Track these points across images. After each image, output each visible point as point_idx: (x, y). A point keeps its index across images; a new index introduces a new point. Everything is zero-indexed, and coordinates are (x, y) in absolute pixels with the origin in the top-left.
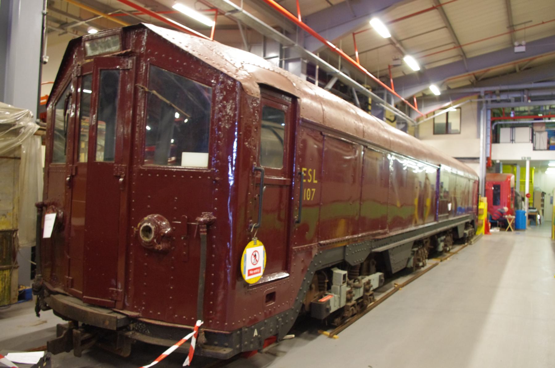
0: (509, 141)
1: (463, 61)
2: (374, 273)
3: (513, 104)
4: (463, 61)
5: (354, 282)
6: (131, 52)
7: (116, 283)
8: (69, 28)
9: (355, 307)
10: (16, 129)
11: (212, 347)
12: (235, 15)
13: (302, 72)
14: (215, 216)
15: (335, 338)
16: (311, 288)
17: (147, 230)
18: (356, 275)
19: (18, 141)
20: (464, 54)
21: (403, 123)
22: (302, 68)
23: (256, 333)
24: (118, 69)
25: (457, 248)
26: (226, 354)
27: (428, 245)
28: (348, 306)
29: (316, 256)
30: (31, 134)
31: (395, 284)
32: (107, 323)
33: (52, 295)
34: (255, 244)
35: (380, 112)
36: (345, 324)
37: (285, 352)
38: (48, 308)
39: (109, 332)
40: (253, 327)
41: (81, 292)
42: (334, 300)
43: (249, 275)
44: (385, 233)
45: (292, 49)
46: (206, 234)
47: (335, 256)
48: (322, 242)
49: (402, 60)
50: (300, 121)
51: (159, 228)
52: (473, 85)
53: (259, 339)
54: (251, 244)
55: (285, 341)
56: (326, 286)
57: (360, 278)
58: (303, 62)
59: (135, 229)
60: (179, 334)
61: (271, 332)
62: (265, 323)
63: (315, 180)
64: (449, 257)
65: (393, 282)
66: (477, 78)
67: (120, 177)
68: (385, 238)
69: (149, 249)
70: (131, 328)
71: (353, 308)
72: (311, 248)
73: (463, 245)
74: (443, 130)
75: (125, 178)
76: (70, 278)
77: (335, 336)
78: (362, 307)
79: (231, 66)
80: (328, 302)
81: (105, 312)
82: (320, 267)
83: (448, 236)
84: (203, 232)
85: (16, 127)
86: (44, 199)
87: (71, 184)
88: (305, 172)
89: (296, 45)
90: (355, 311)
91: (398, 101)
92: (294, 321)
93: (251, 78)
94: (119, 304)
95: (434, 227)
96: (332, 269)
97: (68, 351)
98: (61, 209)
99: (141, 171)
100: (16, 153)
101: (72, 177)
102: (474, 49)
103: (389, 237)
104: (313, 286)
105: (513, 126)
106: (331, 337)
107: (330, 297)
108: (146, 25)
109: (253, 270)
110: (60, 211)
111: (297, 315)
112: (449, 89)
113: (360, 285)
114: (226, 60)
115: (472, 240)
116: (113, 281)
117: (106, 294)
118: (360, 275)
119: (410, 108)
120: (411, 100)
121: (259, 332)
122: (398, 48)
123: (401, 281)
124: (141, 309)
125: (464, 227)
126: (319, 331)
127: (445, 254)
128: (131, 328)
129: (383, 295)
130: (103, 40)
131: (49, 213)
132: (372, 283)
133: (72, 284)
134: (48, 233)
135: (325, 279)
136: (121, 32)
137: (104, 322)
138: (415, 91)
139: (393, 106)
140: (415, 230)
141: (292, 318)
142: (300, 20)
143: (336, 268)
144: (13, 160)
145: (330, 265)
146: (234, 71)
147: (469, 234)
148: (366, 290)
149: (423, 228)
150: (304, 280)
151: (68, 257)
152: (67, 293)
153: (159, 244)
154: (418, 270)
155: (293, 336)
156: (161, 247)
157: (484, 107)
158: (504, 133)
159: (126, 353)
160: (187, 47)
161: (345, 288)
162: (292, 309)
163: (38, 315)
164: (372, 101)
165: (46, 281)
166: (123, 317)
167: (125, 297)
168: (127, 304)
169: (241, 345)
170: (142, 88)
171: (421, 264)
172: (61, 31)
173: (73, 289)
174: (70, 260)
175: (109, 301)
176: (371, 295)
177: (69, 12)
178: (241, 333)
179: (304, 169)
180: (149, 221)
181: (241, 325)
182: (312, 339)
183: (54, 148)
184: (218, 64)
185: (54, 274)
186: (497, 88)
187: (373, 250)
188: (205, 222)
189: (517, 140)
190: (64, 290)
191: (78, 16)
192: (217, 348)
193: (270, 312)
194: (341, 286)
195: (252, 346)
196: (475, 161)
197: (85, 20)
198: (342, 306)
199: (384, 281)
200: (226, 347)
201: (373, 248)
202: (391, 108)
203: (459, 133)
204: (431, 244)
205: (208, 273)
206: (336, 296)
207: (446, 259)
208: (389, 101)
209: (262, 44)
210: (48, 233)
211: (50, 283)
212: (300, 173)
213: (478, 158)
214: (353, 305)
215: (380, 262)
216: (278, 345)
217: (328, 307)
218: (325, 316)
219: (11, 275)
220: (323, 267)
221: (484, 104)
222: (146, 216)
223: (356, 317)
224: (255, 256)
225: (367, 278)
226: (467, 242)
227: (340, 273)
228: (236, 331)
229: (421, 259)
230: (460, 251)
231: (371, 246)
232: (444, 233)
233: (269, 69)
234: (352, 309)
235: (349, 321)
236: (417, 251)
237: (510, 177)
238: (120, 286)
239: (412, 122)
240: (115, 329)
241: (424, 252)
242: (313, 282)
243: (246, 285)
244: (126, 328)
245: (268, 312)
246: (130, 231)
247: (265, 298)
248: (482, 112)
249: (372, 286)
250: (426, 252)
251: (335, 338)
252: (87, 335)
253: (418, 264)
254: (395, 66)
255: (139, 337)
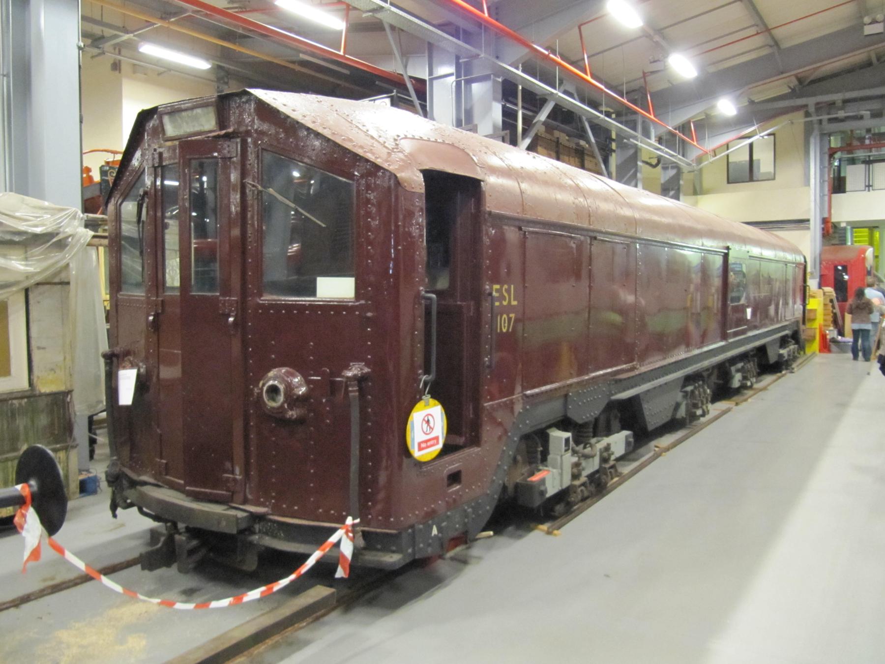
0: (862, 187)
1: (775, 56)
2: (618, 432)
3: (869, 122)
4: (775, 56)
5: (585, 448)
6: (233, 132)
7: (233, 467)
8: (107, 46)
9: (586, 487)
10: (60, 240)
11: (374, 553)
12: (379, 15)
13: (495, 99)
14: (369, 367)
15: (555, 535)
16: (515, 460)
17: (274, 390)
18: (588, 437)
19: (65, 258)
20: (776, 43)
21: (673, 168)
22: (494, 91)
23: (435, 531)
24: (216, 157)
25: (768, 379)
26: (395, 562)
27: (714, 379)
28: (575, 486)
29: (520, 413)
30: (82, 245)
31: (657, 447)
32: (224, 523)
33: (139, 487)
34: (427, 404)
35: (632, 151)
36: (572, 512)
37: (479, 558)
38: (131, 505)
39: (222, 537)
40: (430, 522)
41: (182, 482)
42: (552, 479)
43: (420, 449)
44: (633, 369)
45: (476, 62)
46: (357, 394)
47: (552, 410)
48: (529, 392)
49: (665, 69)
50: (487, 216)
51: (289, 388)
52: (793, 94)
53: (440, 539)
54: (420, 405)
55: (478, 542)
56: (539, 456)
57: (593, 441)
58: (495, 82)
59: (256, 390)
60: (320, 536)
61: (456, 530)
62: (448, 517)
63: (514, 300)
64: (750, 397)
65: (653, 443)
66: (800, 81)
67: (229, 316)
68: (633, 377)
69: (278, 419)
70: (257, 531)
71: (583, 488)
72: (512, 402)
73: (779, 374)
74: (745, 174)
75: (236, 317)
76: (164, 461)
77: (556, 532)
78: (598, 486)
79: (380, 147)
80: (543, 481)
81: (217, 509)
82: (527, 430)
83: (749, 361)
84: (353, 389)
85: (61, 236)
86: (111, 345)
87: (156, 325)
88: (497, 291)
89: (482, 55)
90: (586, 494)
91: (662, 131)
92: (491, 512)
93: (410, 159)
94: (239, 497)
95: (722, 350)
96: (548, 431)
97: (168, 564)
98: (142, 361)
99: (262, 306)
100: (63, 277)
101: (156, 316)
102: (792, 35)
103: (640, 374)
104: (519, 458)
105: (868, 162)
106: (549, 533)
107: (545, 473)
108: (252, 91)
109: (426, 441)
110: (141, 364)
111: (495, 503)
112: (752, 102)
113: (593, 453)
114: (372, 138)
115: (794, 365)
116: (228, 465)
117: (217, 483)
118: (594, 437)
119: (683, 142)
120: (684, 128)
121: (440, 530)
122: (657, 43)
123: (666, 441)
124: (270, 502)
125: (778, 344)
126: (532, 525)
127: (746, 391)
128: (257, 531)
129: (635, 465)
130: (189, 113)
131: (124, 368)
132: (613, 449)
133: (167, 469)
134: (126, 397)
135: (537, 447)
136: (216, 101)
137: (219, 523)
138: (690, 113)
139: (653, 141)
140: (686, 359)
141: (488, 508)
142: (486, 15)
143: (554, 429)
144: (59, 286)
145: (544, 426)
146: (385, 156)
147: (789, 355)
148: (604, 460)
149: (701, 354)
150: (504, 451)
151: (159, 431)
152: (160, 484)
153: (292, 409)
154: (695, 423)
155: (491, 533)
156: (292, 414)
157: (816, 132)
158: (854, 175)
159: (251, 564)
160: (314, 122)
161: (570, 459)
162: (488, 495)
163: (115, 516)
164: (617, 135)
165: (124, 466)
166: (245, 514)
167: (245, 485)
168: (250, 497)
169: (414, 549)
170: (253, 186)
171: (699, 412)
172: (96, 51)
173: (168, 477)
174: (161, 435)
175: (224, 492)
176: (613, 467)
177: (105, 20)
178: (414, 532)
179: (496, 287)
180: (274, 379)
181: (412, 519)
182: (520, 537)
183: (123, 267)
184: (361, 147)
185: (135, 455)
186: (837, 97)
187: (614, 398)
188: (355, 377)
189: (877, 185)
190: (156, 479)
191: (120, 25)
192: (380, 554)
193: (455, 500)
194: (562, 456)
195: (430, 550)
196: (802, 225)
197: (132, 32)
198: (564, 486)
199: (633, 444)
200: (394, 552)
201: (613, 395)
202: (650, 145)
203: (774, 179)
204: (719, 377)
205: (362, 448)
206: (554, 471)
207: (746, 400)
208: (646, 134)
209: (426, 55)
210: (126, 397)
211: (131, 468)
212: (490, 294)
213: (808, 220)
214: (584, 484)
215: (626, 414)
216: (469, 548)
217: (542, 488)
218: (537, 502)
219: (67, 458)
220: (533, 429)
221: (816, 126)
222: (269, 371)
223: (588, 501)
224: (428, 422)
225: (605, 441)
226: (787, 369)
227: (559, 436)
228: (406, 529)
229: (700, 405)
230: (772, 386)
231: (610, 392)
232: (743, 357)
233: (436, 141)
234: (582, 491)
235: (578, 508)
236: (692, 392)
237: (864, 251)
238: (237, 470)
239: (689, 165)
240: (235, 532)
241: (705, 392)
242: (518, 450)
243: (419, 464)
244: (250, 530)
245: (451, 500)
246: (248, 393)
247: (446, 480)
248: (812, 140)
249: (613, 454)
250: (708, 391)
251: (555, 535)
252: (194, 543)
253: (695, 413)
254: (653, 73)
255: (269, 542)
